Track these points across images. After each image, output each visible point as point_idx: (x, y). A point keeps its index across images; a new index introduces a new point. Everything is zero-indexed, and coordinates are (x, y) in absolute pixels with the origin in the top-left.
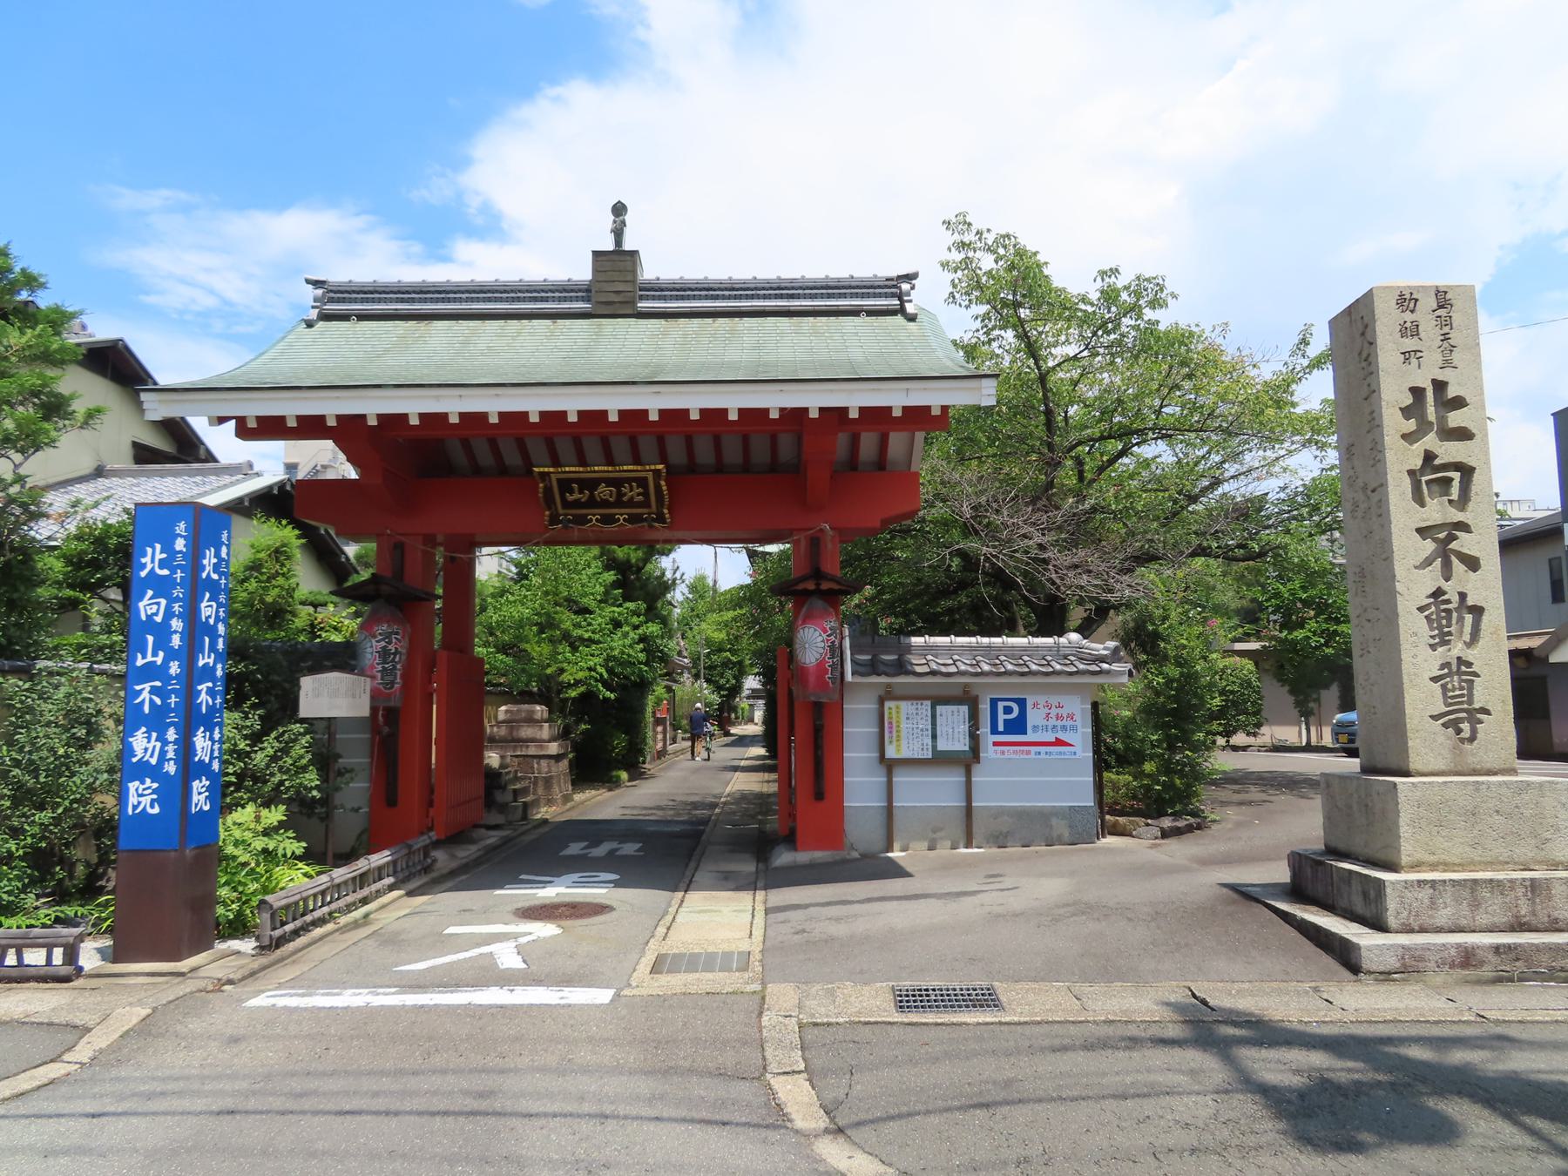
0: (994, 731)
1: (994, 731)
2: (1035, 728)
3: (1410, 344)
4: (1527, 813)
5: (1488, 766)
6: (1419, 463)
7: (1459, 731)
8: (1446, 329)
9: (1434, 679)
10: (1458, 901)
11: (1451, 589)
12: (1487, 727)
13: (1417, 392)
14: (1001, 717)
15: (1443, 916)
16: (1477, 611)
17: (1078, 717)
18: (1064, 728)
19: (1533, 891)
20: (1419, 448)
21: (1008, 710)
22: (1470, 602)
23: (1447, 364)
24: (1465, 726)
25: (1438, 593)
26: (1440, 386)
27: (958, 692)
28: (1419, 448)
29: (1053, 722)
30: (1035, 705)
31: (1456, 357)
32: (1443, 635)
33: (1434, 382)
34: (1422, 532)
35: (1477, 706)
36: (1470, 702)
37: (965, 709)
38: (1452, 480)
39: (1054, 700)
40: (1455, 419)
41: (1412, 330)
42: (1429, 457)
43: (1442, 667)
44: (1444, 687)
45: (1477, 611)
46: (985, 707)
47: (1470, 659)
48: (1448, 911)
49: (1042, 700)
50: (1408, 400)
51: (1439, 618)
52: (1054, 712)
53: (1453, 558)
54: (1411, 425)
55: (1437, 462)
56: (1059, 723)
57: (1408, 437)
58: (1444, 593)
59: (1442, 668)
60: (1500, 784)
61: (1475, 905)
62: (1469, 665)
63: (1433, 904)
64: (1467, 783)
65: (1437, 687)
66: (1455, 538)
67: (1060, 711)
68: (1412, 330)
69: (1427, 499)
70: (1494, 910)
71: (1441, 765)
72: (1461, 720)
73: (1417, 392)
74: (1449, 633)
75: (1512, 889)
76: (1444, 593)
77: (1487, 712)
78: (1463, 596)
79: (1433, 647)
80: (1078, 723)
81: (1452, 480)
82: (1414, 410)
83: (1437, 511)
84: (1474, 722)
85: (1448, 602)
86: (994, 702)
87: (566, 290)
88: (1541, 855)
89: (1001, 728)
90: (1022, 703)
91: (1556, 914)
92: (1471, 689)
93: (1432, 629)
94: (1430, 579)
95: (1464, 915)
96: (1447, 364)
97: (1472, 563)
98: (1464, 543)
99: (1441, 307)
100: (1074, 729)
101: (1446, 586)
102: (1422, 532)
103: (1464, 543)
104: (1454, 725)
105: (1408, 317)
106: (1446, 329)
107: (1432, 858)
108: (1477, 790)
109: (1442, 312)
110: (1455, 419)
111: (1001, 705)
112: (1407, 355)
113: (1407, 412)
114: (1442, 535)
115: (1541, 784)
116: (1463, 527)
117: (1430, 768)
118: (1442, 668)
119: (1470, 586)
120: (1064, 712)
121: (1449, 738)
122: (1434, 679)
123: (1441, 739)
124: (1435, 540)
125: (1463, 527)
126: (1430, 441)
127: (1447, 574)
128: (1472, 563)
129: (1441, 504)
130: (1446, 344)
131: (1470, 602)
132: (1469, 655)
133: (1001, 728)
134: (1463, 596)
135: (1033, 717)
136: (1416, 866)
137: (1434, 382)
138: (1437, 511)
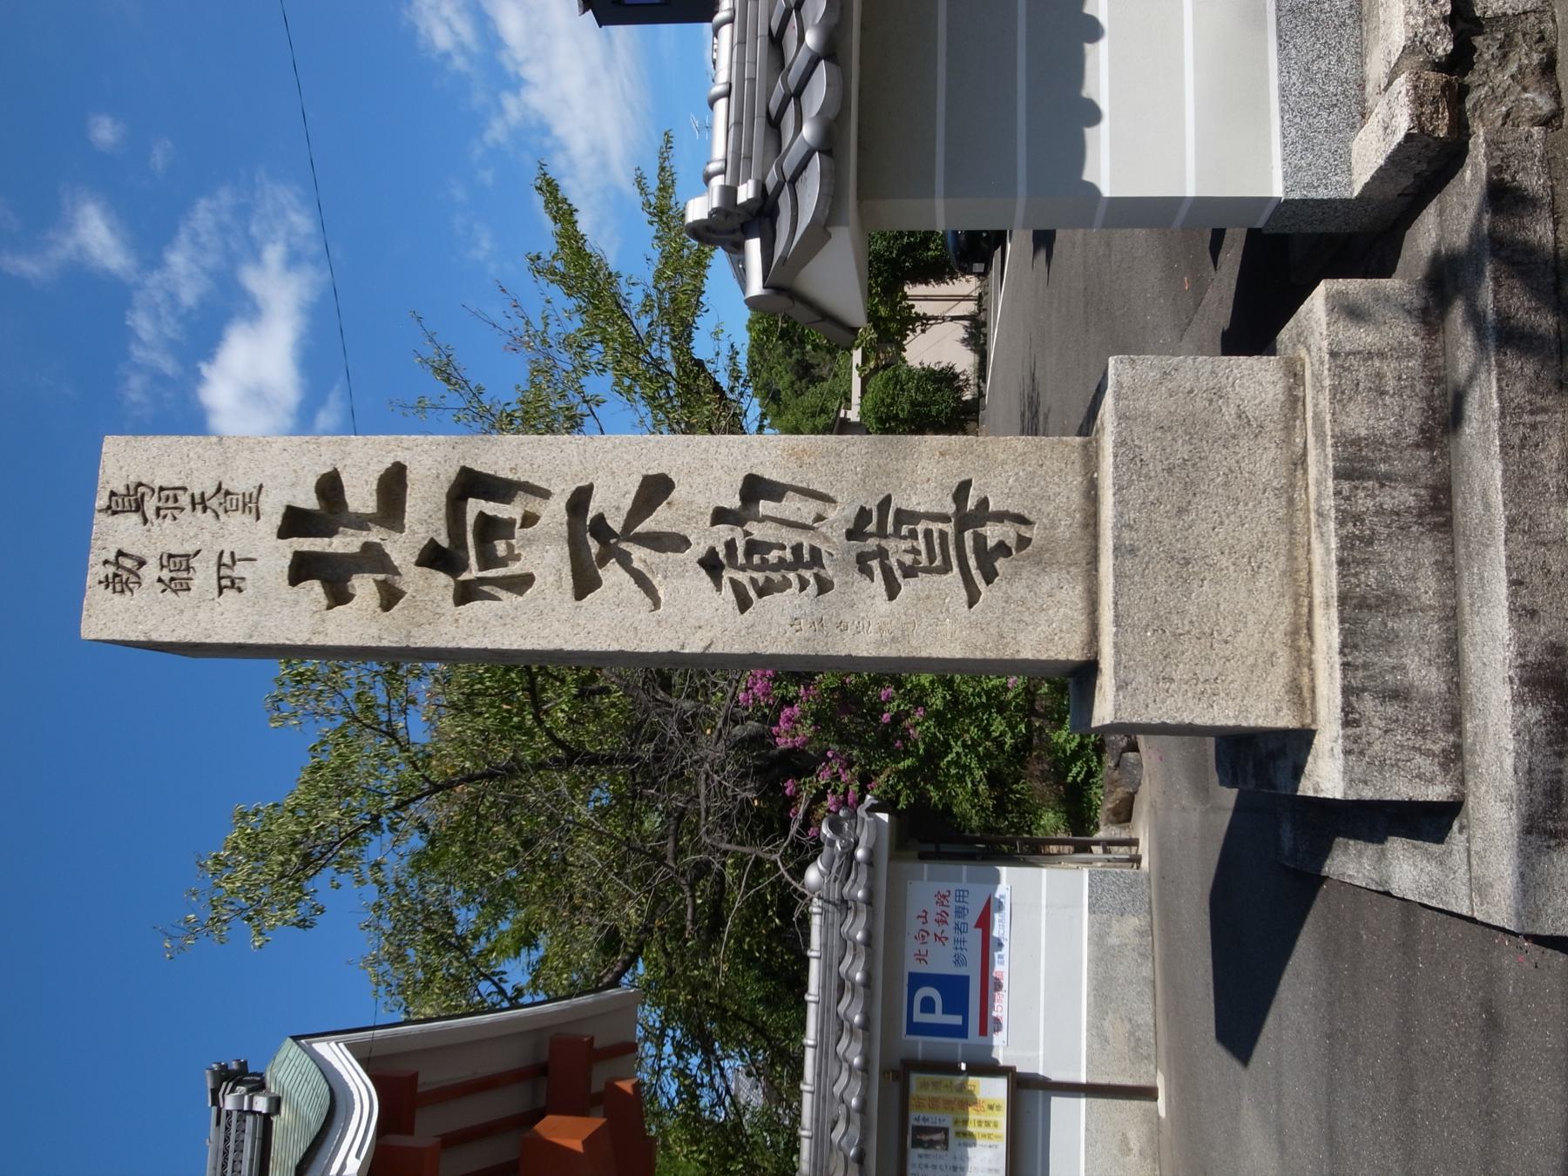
0: (961, 1031)
1: (961, 1031)
2: (959, 961)
3: (204, 575)
4: (1183, 451)
5: (1076, 499)
6: (442, 579)
7: (1003, 549)
8: (184, 499)
9: (892, 591)
10: (1389, 640)
11: (706, 538)
12: (997, 490)
13: (302, 569)
14: (939, 1017)
15: (1425, 676)
16: (755, 489)
17: (943, 887)
18: (960, 912)
19: (1364, 476)
20: (413, 578)
21: (928, 1005)
22: (734, 502)
23: (251, 504)
24: (994, 533)
25: (711, 565)
26: (295, 522)
27: (896, 1088)
28: (413, 578)
29: (949, 931)
30: (921, 958)
31: (240, 484)
32: (798, 563)
33: (284, 533)
34: (585, 583)
35: (950, 508)
36: (944, 518)
37: (915, 1079)
38: (481, 514)
39: (913, 926)
40: (361, 496)
41: (178, 568)
42: (435, 557)
43: (866, 571)
44: (909, 572)
45: (755, 489)
46: (922, 1045)
47: (852, 512)
48: (1412, 663)
49: (912, 946)
50: (314, 589)
51: (764, 566)
52: (933, 927)
53: (638, 529)
54: (364, 586)
55: (444, 541)
56: (951, 919)
57: (390, 597)
58: (712, 552)
59: (869, 573)
60: (1121, 502)
61: (1390, 601)
62: (863, 515)
63: (1398, 695)
64: (1119, 576)
65: (907, 587)
66: (600, 518)
67: (931, 918)
68: (178, 568)
69: (515, 569)
70: (1410, 565)
71: (1073, 594)
72: (980, 540)
73: (302, 569)
74: (797, 549)
75: (1358, 519)
76: (712, 552)
77: (963, 490)
78: (720, 516)
79: (824, 586)
80: (953, 887)
81: (481, 514)
82: (333, 577)
83: (543, 555)
84: (983, 514)
85: (731, 546)
86: (914, 1028)
87: (526, 492)
88: (1274, 430)
89: (956, 1020)
90: (917, 980)
91: (1412, 434)
92: (914, 517)
93: (786, 584)
94: (681, 580)
95: (1421, 629)
96: (251, 504)
97: (655, 490)
98: (614, 502)
99: (139, 507)
100: (961, 895)
101: (698, 550)
102: (585, 583)
103: (614, 502)
104: (988, 558)
105: (150, 572)
106: (184, 499)
107: (1283, 656)
108: (1133, 551)
109: (150, 505)
110: (361, 496)
111: (919, 1017)
112: (228, 583)
113: (339, 595)
114: (594, 547)
115: (1122, 417)
116: (579, 500)
117: (1079, 616)
118: (869, 573)
119: (700, 500)
120: (933, 911)
121: (1016, 573)
122: (892, 591)
123: (1019, 589)
124: (603, 560)
125: (579, 500)
126: (401, 549)
127: (673, 542)
128: (655, 490)
129: (530, 542)
130: (214, 503)
131: (734, 502)
132: (840, 516)
133: (956, 1020)
134: (720, 516)
135: (940, 962)
136: (1300, 693)
137: (284, 533)
138: (543, 555)
